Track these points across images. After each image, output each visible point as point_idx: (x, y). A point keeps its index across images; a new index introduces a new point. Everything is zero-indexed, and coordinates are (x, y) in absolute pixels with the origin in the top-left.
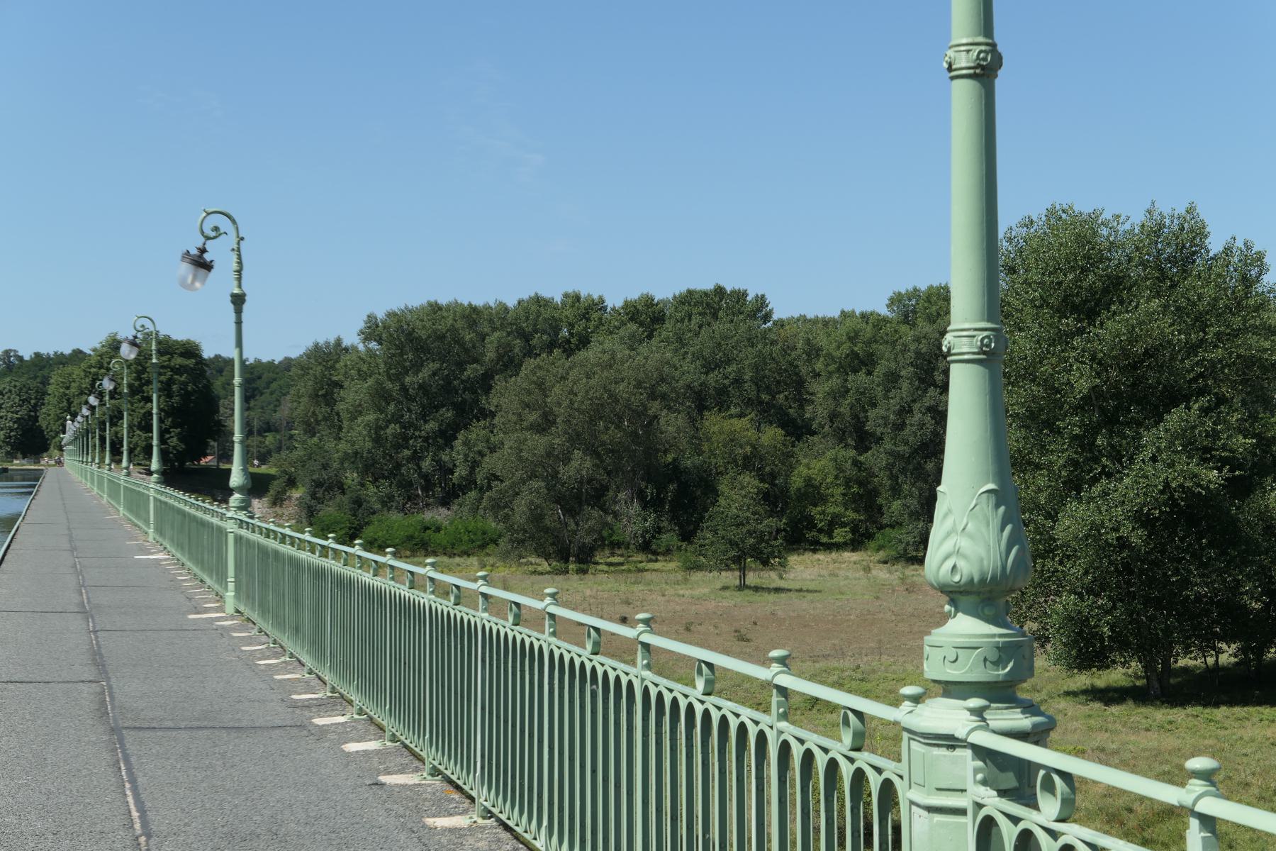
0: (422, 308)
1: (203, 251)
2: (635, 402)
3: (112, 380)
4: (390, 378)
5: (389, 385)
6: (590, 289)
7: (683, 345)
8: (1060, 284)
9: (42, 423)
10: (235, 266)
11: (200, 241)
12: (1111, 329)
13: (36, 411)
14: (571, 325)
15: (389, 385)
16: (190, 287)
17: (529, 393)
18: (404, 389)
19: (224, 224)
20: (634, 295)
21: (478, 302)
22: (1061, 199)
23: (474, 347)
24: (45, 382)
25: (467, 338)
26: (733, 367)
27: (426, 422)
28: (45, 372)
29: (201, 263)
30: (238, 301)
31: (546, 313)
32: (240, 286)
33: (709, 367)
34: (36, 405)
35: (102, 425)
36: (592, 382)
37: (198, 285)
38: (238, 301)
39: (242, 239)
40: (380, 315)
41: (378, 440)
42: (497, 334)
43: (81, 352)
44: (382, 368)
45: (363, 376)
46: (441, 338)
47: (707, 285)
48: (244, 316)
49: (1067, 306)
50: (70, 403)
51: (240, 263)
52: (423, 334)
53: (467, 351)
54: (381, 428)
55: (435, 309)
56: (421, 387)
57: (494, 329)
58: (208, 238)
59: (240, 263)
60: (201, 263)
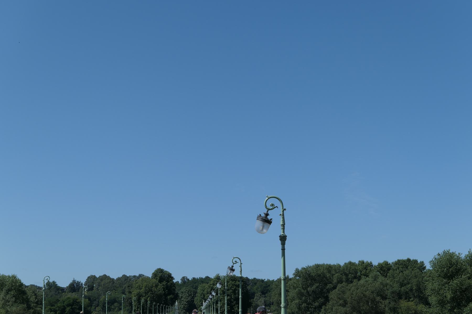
0: (313, 266)
1: (233, 267)
2: (371, 297)
3: (220, 284)
4: (303, 288)
5: (303, 291)
6: (367, 259)
7: (394, 278)
8: (443, 271)
9: (196, 303)
10: (281, 223)
11: (265, 211)
12: (455, 282)
13: (193, 298)
14: (361, 271)
15: (303, 291)
16: (261, 232)
17: (340, 294)
18: (308, 292)
19: (277, 203)
20: (381, 261)
21: (332, 263)
22: (446, 249)
23: (330, 278)
24: (196, 288)
25: (328, 276)
26: (410, 285)
27: (315, 303)
28: (196, 284)
29: (267, 221)
30: (283, 239)
31: (353, 267)
32: (284, 232)
33: (402, 285)
34: (193, 296)
35: (214, 303)
36: (358, 291)
37: (265, 231)
38: (283, 239)
39: (285, 209)
40: (300, 269)
41: (299, 308)
42: (337, 274)
43: (208, 277)
44: (301, 286)
45: (295, 288)
46: (319, 276)
47: (405, 258)
48: (286, 246)
49: (446, 276)
50: (204, 296)
51: (284, 221)
52: (313, 275)
53: (328, 280)
54: (300, 305)
55: (318, 266)
56: (313, 291)
57: (337, 273)
58: (269, 210)
59: (284, 221)
60: (267, 221)
